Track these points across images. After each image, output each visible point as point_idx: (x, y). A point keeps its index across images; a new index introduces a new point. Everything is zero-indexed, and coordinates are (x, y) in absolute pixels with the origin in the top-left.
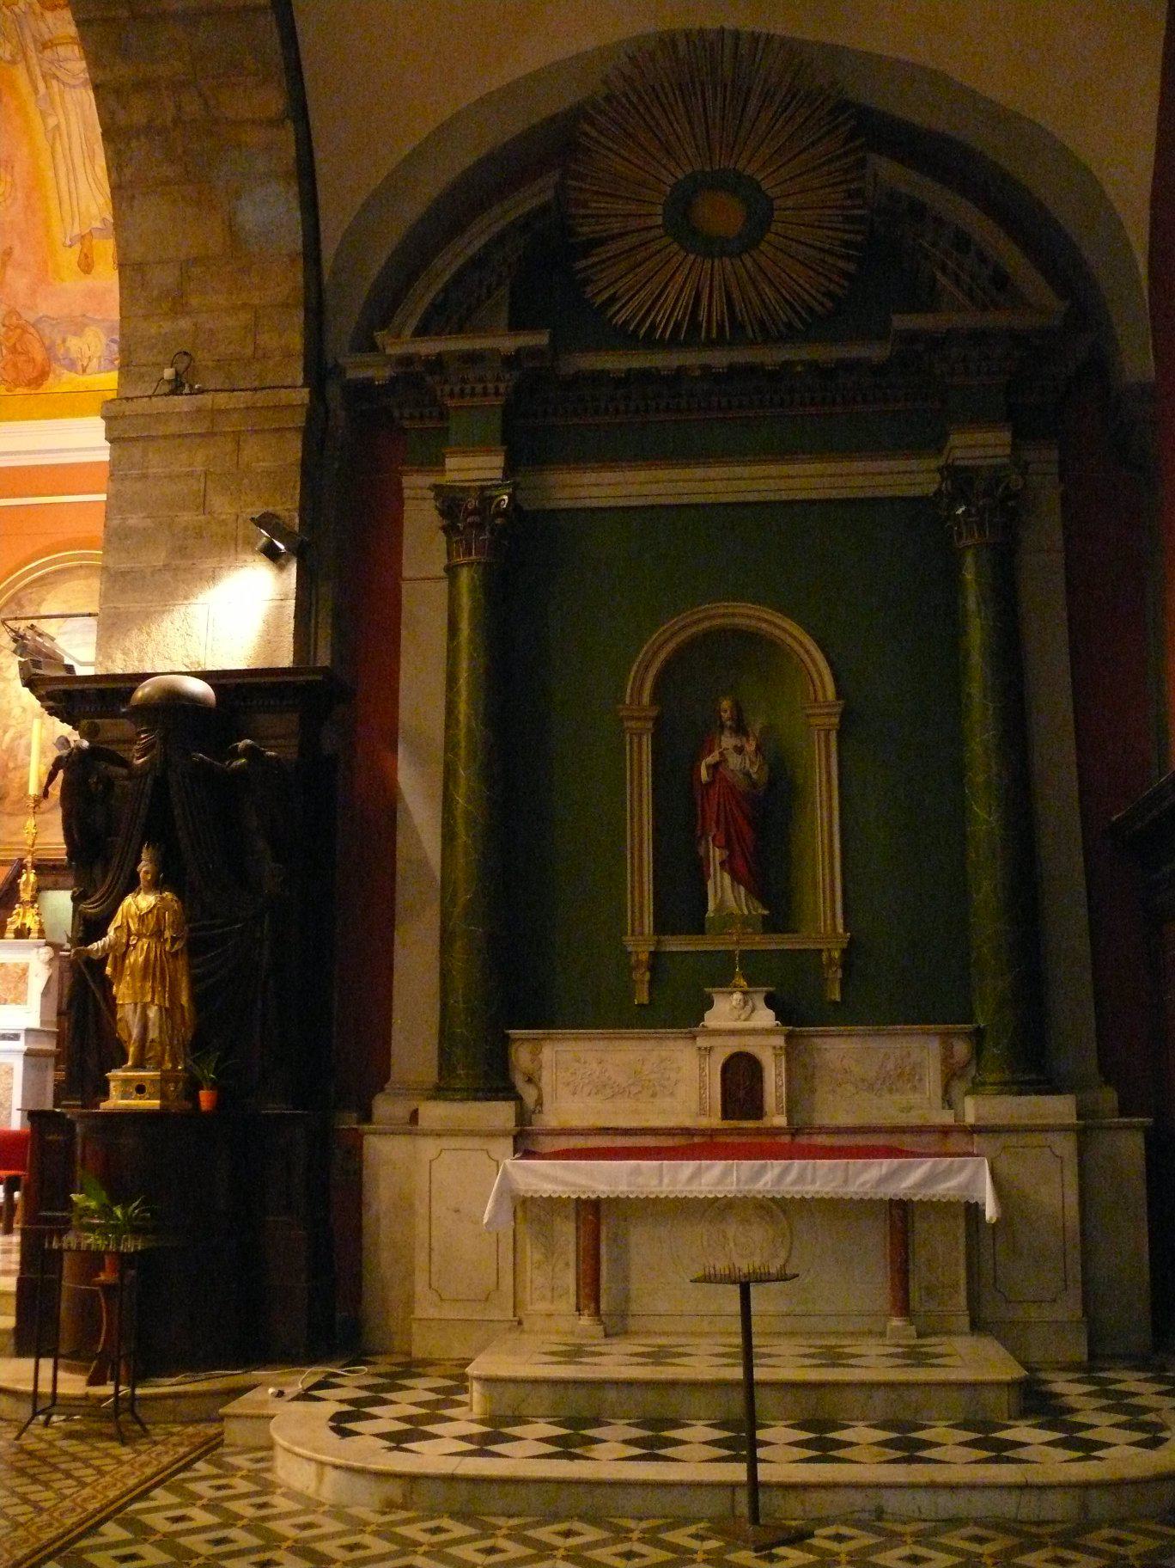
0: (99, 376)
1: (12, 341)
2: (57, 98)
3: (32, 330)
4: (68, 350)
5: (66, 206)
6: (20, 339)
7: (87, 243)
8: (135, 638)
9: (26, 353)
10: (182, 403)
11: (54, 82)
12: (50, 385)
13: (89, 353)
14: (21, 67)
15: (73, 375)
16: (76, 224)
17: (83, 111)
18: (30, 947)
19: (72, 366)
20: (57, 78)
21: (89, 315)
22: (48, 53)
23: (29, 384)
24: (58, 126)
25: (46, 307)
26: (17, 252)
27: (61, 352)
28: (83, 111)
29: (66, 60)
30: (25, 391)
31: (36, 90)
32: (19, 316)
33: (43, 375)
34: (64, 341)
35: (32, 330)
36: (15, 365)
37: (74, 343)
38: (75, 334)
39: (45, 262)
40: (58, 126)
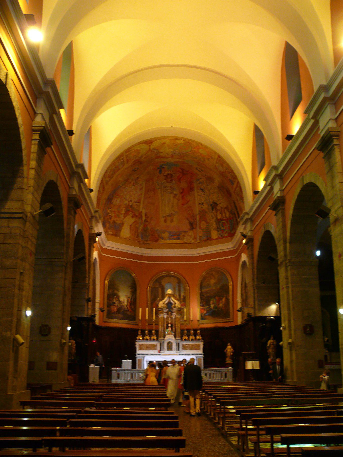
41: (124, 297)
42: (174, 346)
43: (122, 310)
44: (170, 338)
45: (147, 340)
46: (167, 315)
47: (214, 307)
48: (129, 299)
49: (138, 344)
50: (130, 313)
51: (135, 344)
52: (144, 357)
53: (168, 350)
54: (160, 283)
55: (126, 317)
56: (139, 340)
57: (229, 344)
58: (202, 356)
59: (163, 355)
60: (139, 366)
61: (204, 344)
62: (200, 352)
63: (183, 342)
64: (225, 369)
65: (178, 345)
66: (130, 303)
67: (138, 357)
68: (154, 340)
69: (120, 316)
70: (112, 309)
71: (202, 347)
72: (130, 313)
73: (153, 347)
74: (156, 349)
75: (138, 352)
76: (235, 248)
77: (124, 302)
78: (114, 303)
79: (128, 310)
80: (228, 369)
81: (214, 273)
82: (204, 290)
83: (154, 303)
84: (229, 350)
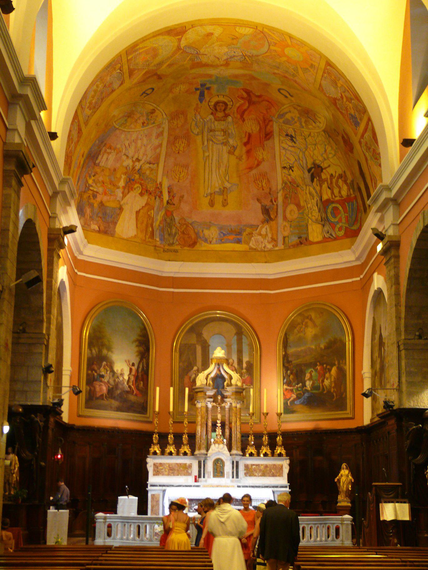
0: (216, 245)
1: (183, 229)
2: (210, 147)
3: (190, 226)
4: (204, 235)
5: (206, 183)
6: (185, 229)
7: (213, 196)
8: (415, 398)
9: (188, 234)
10: (422, 341)
11: (211, 142)
12: (197, 247)
13: (212, 236)
14: (200, 137)
15: (206, 244)
16: (209, 189)
17: (219, 152)
18: (283, 460)
19: (206, 240)
20: (212, 141)
21: (213, 222)
22: (211, 133)
23: (189, 246)
24: (209, 156)
25: (195, 218)
26: (185, 198)
27: (201, 235)
28: (219, 152)
29: (217, 135)
30: (188, 249)
31: (203, 144)
32: (185, 220)
33: (194, 244)
34: (203, 231)
35: (190, 226)
36: (184, 239)
37: (206, 232)
38: (207, 229)
39: (196, 201)
40: (209, 156)
42: (228, 468)
44: (219, 450)
47: (313, 387)
48: (134, 368)
49: (151, 462)
51: (146, 463)
52: (164, 491)
54: (199, 335)
56: (155, 453)
59: (204, 486)
60: (152, 510)
62: (283, 480)
63: (247, 459)
64: (337, 520)
65: (236, 465)
66: (137, 378)
68: (185, 454)
69: (115, 403)
70: (98, 389)
73: (184, 470)
74: (190, 474)
75: (152, 479)
77: (122, 374)
78: (103, 376)
79: (131, 392)
80: (343, 520)
81: (313, 315)
84: (343, 479)
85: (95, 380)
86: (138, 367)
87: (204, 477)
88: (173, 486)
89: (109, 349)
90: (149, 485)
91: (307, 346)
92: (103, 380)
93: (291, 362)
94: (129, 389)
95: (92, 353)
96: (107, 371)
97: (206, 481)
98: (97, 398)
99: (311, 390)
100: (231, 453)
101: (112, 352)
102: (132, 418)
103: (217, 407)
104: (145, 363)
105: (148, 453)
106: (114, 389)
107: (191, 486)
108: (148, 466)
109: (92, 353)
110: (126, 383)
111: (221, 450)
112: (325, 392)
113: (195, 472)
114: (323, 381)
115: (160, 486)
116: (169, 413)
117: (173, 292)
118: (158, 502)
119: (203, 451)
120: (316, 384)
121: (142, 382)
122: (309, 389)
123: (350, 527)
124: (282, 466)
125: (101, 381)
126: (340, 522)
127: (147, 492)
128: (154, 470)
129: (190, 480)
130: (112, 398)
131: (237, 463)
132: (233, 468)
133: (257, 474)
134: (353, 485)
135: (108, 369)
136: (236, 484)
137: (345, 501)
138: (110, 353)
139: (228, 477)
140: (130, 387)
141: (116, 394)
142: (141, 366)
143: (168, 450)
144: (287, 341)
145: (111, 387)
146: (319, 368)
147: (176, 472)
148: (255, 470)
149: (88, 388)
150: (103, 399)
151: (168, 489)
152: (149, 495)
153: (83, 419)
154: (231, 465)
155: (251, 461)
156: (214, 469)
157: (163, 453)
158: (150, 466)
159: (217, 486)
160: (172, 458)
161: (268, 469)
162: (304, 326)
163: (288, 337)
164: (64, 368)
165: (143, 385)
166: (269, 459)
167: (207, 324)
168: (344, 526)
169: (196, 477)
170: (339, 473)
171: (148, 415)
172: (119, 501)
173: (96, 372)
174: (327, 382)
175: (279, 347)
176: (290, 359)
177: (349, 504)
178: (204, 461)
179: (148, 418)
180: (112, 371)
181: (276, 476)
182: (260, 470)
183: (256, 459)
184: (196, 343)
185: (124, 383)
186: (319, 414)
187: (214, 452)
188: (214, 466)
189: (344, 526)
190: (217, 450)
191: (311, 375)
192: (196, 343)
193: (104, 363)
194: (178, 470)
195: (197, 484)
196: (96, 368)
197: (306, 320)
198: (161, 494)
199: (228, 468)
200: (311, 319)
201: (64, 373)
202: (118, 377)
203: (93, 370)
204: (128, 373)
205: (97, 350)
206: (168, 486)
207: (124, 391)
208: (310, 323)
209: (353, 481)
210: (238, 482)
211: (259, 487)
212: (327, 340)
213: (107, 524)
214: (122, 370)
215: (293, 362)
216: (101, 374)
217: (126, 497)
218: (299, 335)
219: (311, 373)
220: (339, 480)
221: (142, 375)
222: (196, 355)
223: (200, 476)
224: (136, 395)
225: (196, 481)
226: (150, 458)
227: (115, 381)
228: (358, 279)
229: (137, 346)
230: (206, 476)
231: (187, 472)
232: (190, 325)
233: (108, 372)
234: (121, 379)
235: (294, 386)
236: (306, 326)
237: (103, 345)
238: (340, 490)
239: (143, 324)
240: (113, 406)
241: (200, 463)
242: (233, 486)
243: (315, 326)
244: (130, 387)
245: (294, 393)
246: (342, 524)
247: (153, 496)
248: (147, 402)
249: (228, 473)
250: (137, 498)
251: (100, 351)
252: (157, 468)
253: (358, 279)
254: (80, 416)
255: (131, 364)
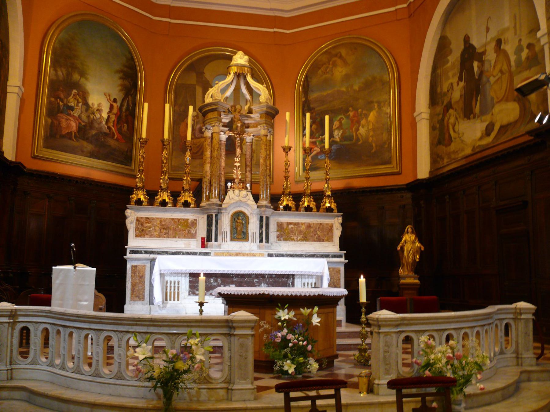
41: (100, 96)
42: (253, 227)
43: (94, 132)
44: (238, 199)
45: (164, 204)
46: (230, 130)
47: (344, 138)
48: (116, 106)
49: (132, 215)
50: (117, 140)
51: (125, 218)
52: (153, 261)
53: (233, 239)
54: (200, 74)
55: (102, 151)
56: (139, 202)
57: (409, 228)
58: (343, 259)
59: (217, 254)
60: (133, 290)
61: (342, 225)
62: (333, 247)
63: (281, 215)
64: (507, 312)
65: (264, 222)
66: (119, 118)
67: (132, 261)
68: (186, 204)
69: (89, 147)
70: (64, 124)
71: (337, 232)
72: (117, 140)
73: (184, 229)
74: (193, 236)
75: (133, 242)
76: (83, 371)
77: (99, 110)
78: (72, 108)
79: (110, 135)
80: (520, 312)
81: (343, 52)
82: (313, 96)
83: (184, 95)
84: (408, 247)
85: (60, 111)
86: (122, 105)
87: (216, 240)
88: (166, 253)
89: (83, 74)
90: (128, 252)
91: (336, 89)
92: (72, 113)
93: (314, 109)
94: (108, 131)
95: (56, 75)
96: (78, 102)
97: (219, 246)
98: (63, 136)
99: (341, 141)
100: (259, 204)
101: (86, 79)
102: (111, 168)
103: (236, 138)
104: (130, 102)
105: (129, 202)
106: (88, 128)
107: (195, 254)
108: (127, 222)
109: (56, 75)
110: (104, 123)
111: (242, 199)
112: (360, 143)
113: (202, 231)
114: (357, 130)
115: (146, 252)
116: (163, 141)
117: (170, 22)
118: (142, 277)
119: (215, 201)
120: (347, 134)
121: (125, 125)
122: (338, 140)
123: (531, 325)
124: (332, 226)
125: (69, 115)
126: (511, 316)
127: (125, 262)
128: (137, 229)
129: (194, 245)
130: (83, 140)
131: (268, 218)
132: (261, 227)
133: (295, 238)
134: (422, 254)
135: (80, 100)
136: (265, 252)
137: (410, 277)
138: (83, 80)
139: (254, 241)
140: (109, 128)
141: (90, 135)
142: (125, 105)
143: (159, 199)
144: (308, 85)
145: (83, 124)
146: (351, 114)
147: (171, 232)
148: (292, 232)
149: (50, 121)
150: (71, 139)
151: (159, 257)
152: (129, 266)
153: (41, 162)
154: (258, 223)
155: (286, 218)
156: (232, 227)
157: (151, 202)
158: (131, 223)
159: (237, 254)
160: (166, 211)
161: (312, 230)
162: (331, 66)
163: (309, 79)
164: (9, 83)
165: (128, 129)
166: (313, 216)
167: (210, 62)
168: (521, 325)
169: (203, 239)
170: (402, 238)
171: (133, 167)
172: (54, 276)
173: (62, 101)
174: (362, 131)
175: (298, 91)
176: (312, 106)
177: (417, 281)
178: (216, 216)
179: (132, 170)
180: (86, 103)
181: (323, 241)
182: (300, 232)
183: (295, 216)
184: (195, 83)
185: (101, 122)
186: (350, 170)
187: (232, 201)
188: (232, 223)
189: (521, 325)
190: (237, 199)
191: (341, 122)
192: (195, 83)
193: (75, 91)
194: (175, 230)
195: (204, 250)
196: (62, 96)
197: (334, 59)
198: (148, 265)
199: (253, 227)
200: (341, 57)
201: (9, 89)
202: (93, 113)
203: (57, 97)
204: (108, 110)
205: (65, 72)
206: (159, 253)
207: (101, 133)
208: (339, 62)
209: (423, 249)
210: (269, 248)
211: (313, 256)
212: (363, 80)
213: (19, 326)
214: (99, 105)
215: (316, 109)
216: (70, 104)
217: (71, 267)
218: (324, 76)
219: (340, 121)
220: (402, 248)
221: (126, 116)
222: (195, 98)
223: (209, 239)
224: (117, 140)
225: (203, 246)
226: (131, 209)
227: (88, 117)
228: (405, 5)
229: (121, 78)
230: (220, 238)
231: (189, 232)
232: (190, 62)
233: (80, 104)
234: (98, 116)
235: (316, 138)
236: (335, 65)
237: (74, 67)
238: (404, 261)
239: (130, 53)
240: (85, 150)
241: (209, 218)
242: (262, 255)
243: (345, 63)
244: (109, 128)
245: (317, 146)
246: (515, 319)
247: (134, 267)
248: (131, 151)
249: (254, 234)
250: (95, 269)
251: (69, 75)
252: (142, 225)
253: (405, 5)
254: (35, 157)
255: (112, 99)
